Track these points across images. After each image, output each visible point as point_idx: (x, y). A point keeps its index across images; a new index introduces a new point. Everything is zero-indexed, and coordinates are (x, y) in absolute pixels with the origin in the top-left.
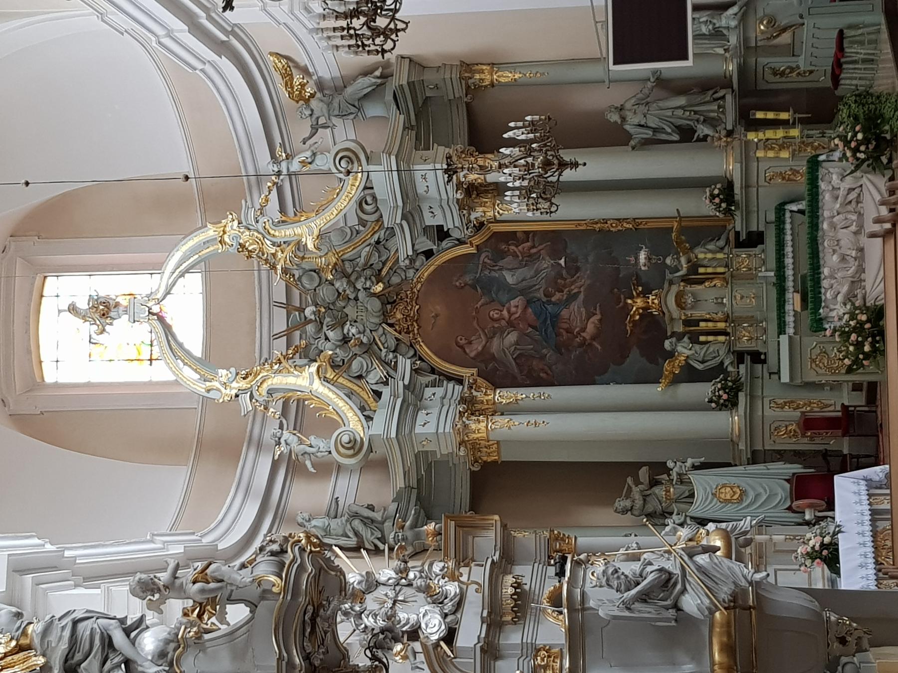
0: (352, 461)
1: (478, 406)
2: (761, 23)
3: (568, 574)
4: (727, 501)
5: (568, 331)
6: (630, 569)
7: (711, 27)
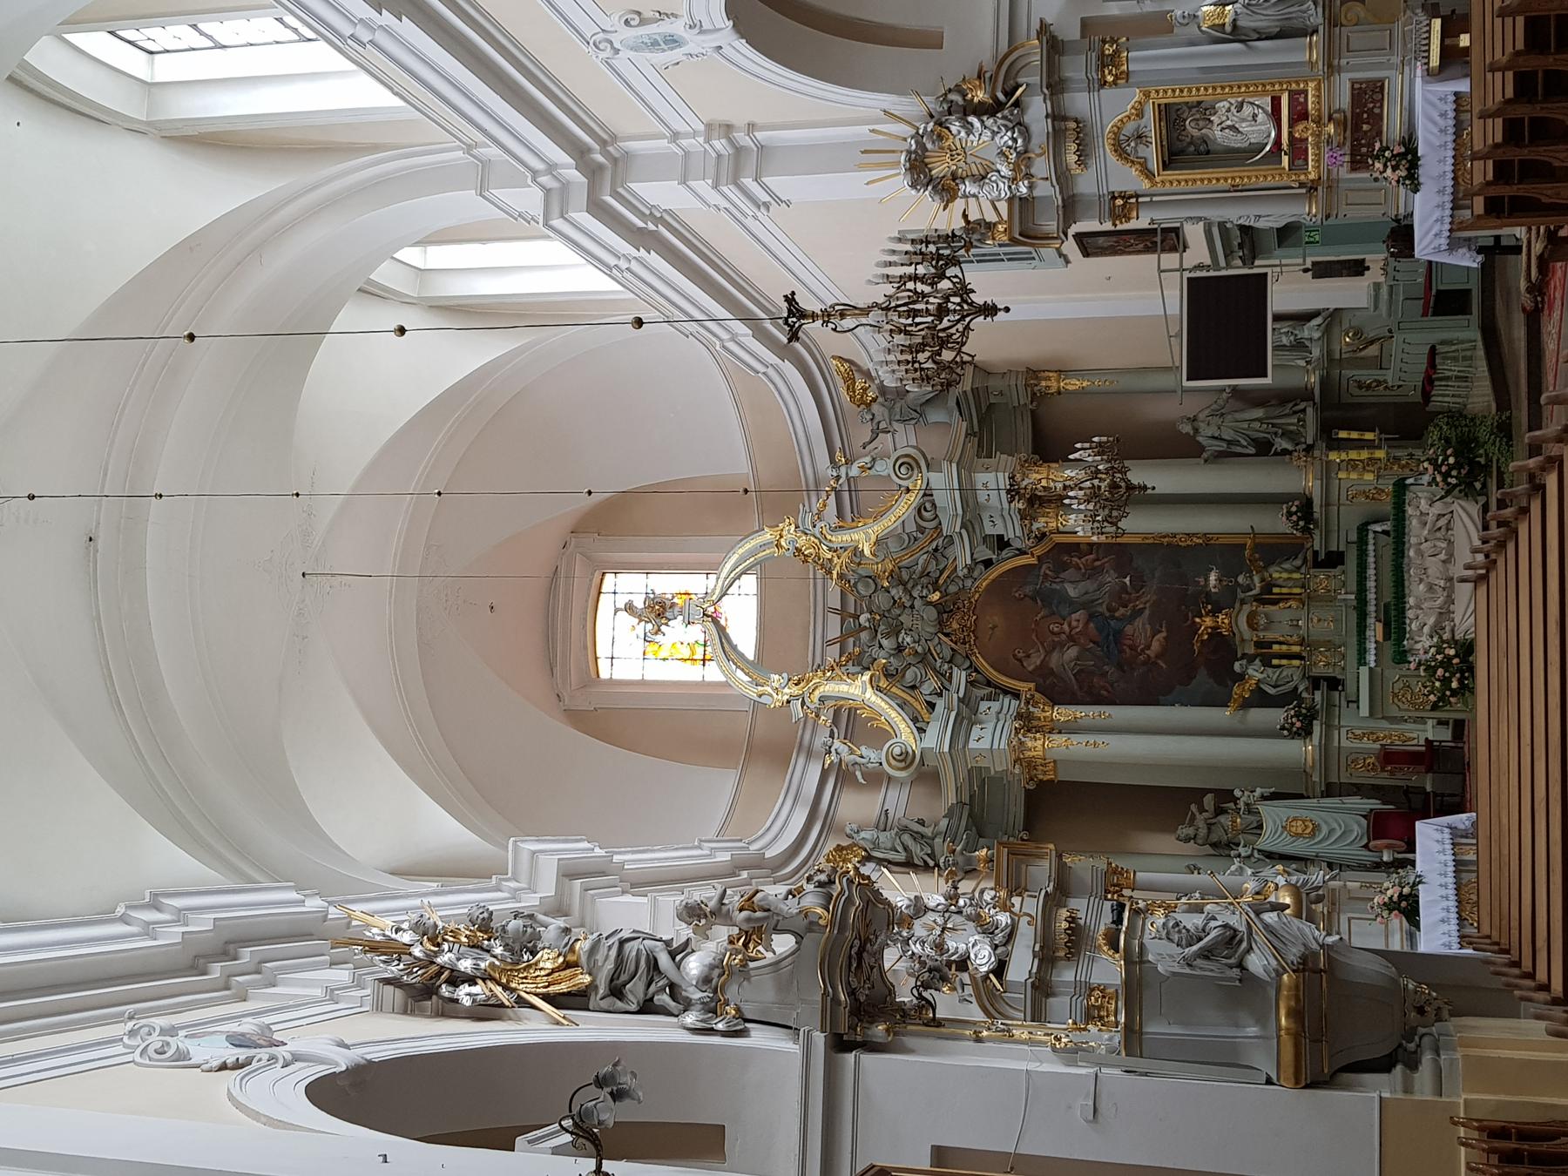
0: (903, 774)
1: (1035, 723)
3: (1125, 922)
4: (1298, 835)
6: (1193, 921)
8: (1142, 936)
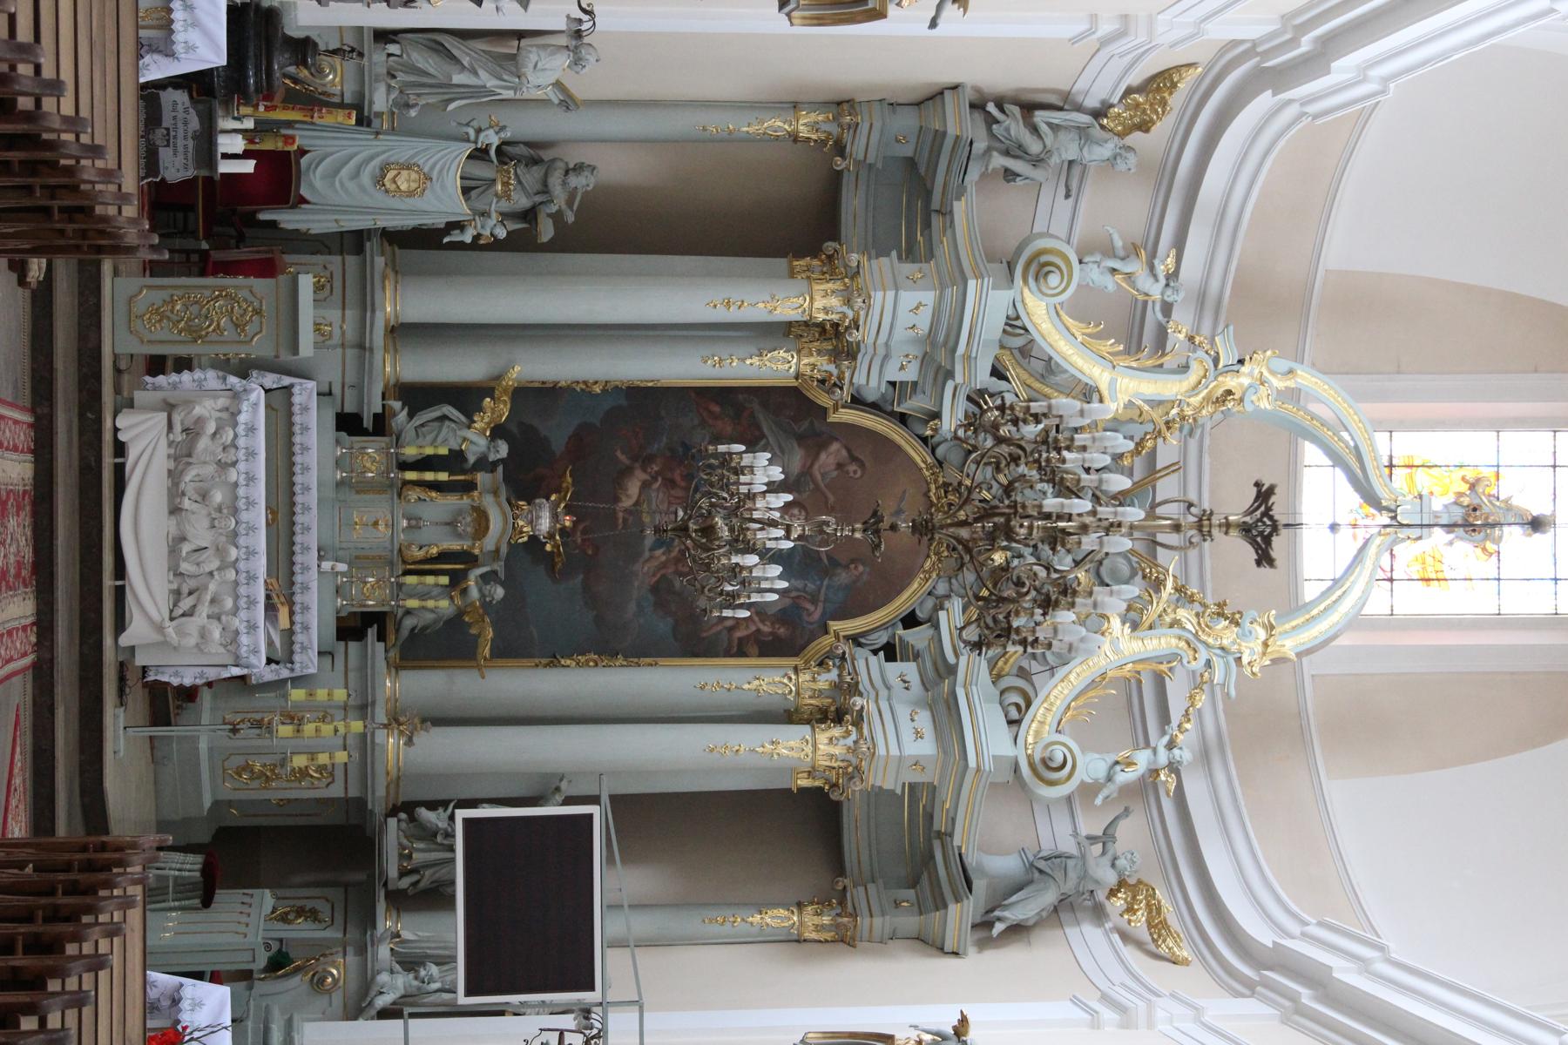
2: (336, 981)
7: (423, 973)
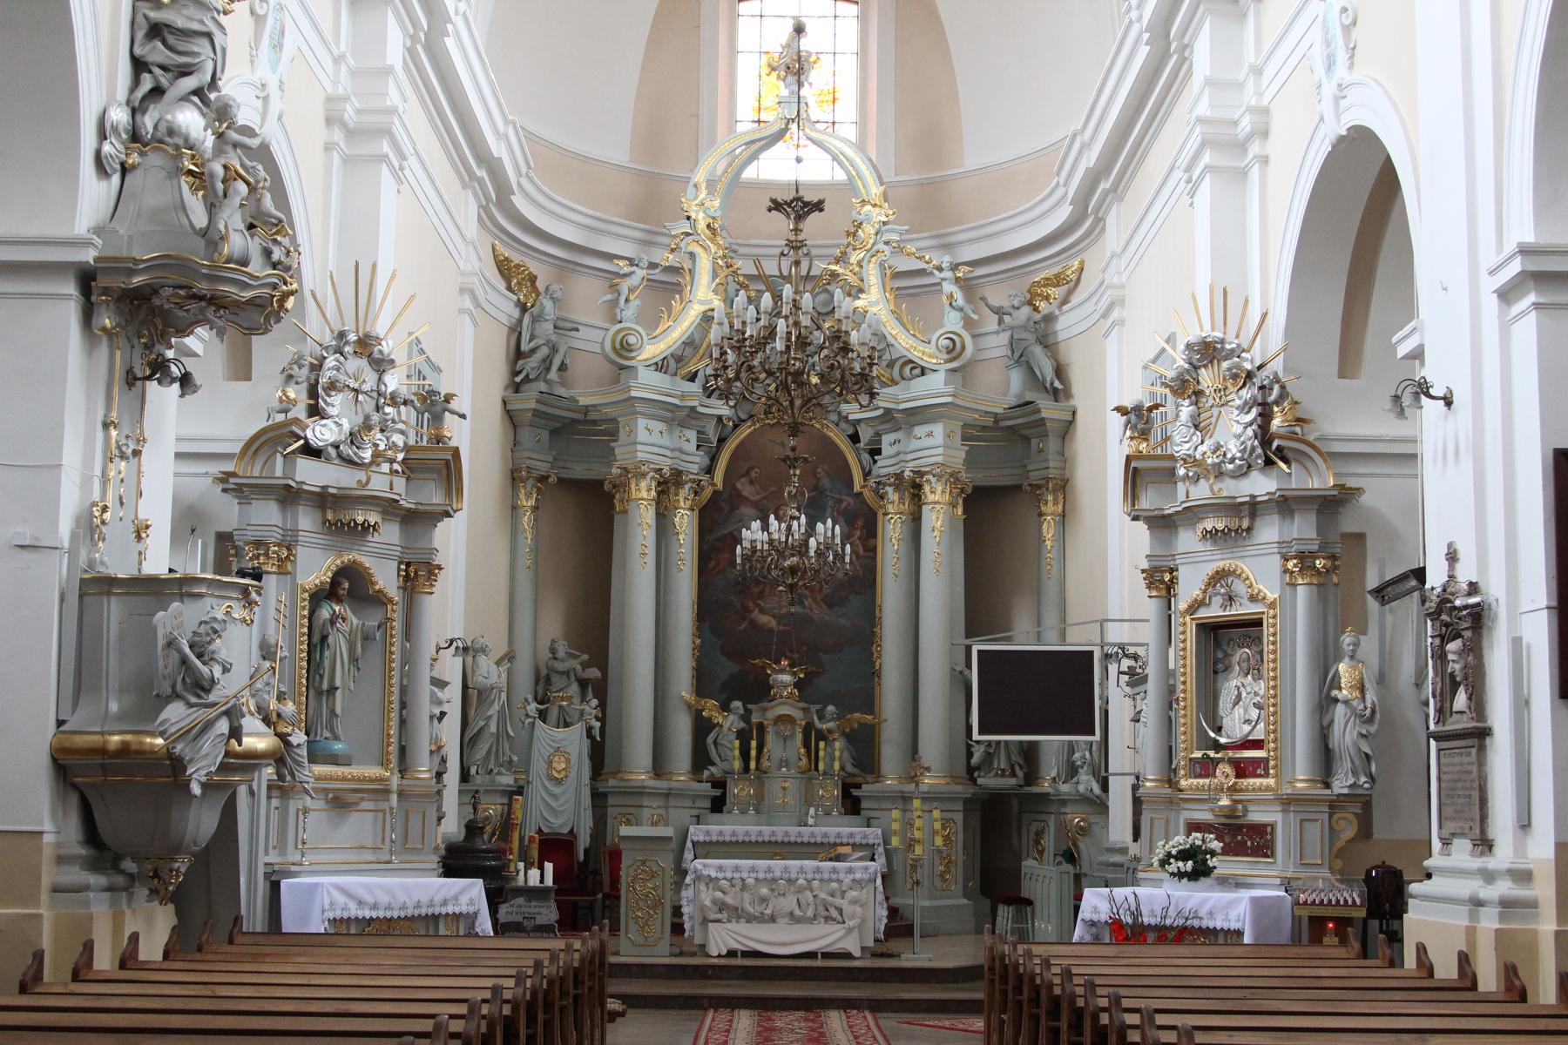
5: (762, 593)
8: (212, 595)
